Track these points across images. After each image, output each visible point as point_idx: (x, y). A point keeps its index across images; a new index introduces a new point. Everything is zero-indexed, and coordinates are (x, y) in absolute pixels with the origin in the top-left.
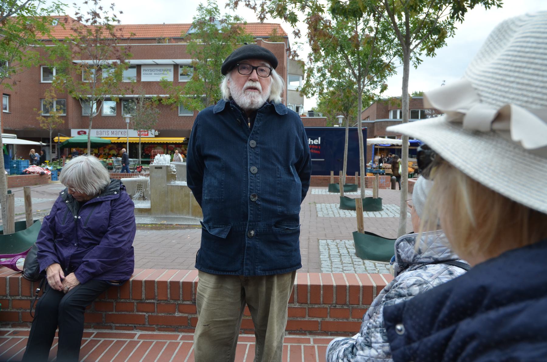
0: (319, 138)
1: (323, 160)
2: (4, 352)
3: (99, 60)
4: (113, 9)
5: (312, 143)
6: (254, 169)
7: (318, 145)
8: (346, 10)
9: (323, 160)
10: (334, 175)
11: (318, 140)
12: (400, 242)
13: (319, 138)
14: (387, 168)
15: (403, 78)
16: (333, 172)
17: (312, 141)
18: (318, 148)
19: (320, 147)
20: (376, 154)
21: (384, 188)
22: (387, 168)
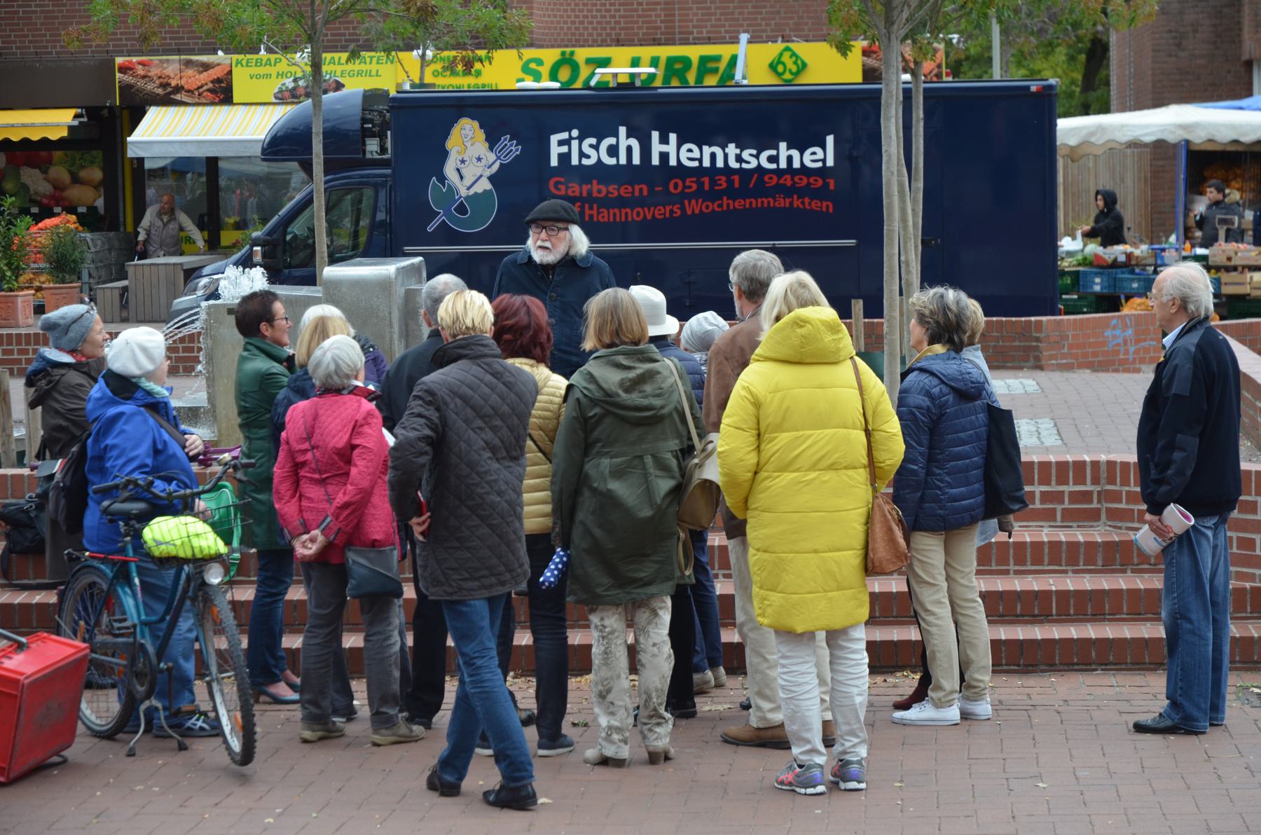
0: (830, 140)
1: (751, 186)
3: (261, 41)
4: (1140, 728)
5: (796, 165)
6: (481, 783)
7: (823, 171)
8: (213, 245)
9: (751, 186)
10: (865, 317)
11: (824, 148)
12: (1037, 616)
13: (830, 140)
14: (1235, 269)
15: (376, 89)
16: (861, 302)
17: (795, 153)
18: (826, 185)
19: (832, 183)
20: (1195, 186)
21: (1127, 371)
22: (1235, 269)
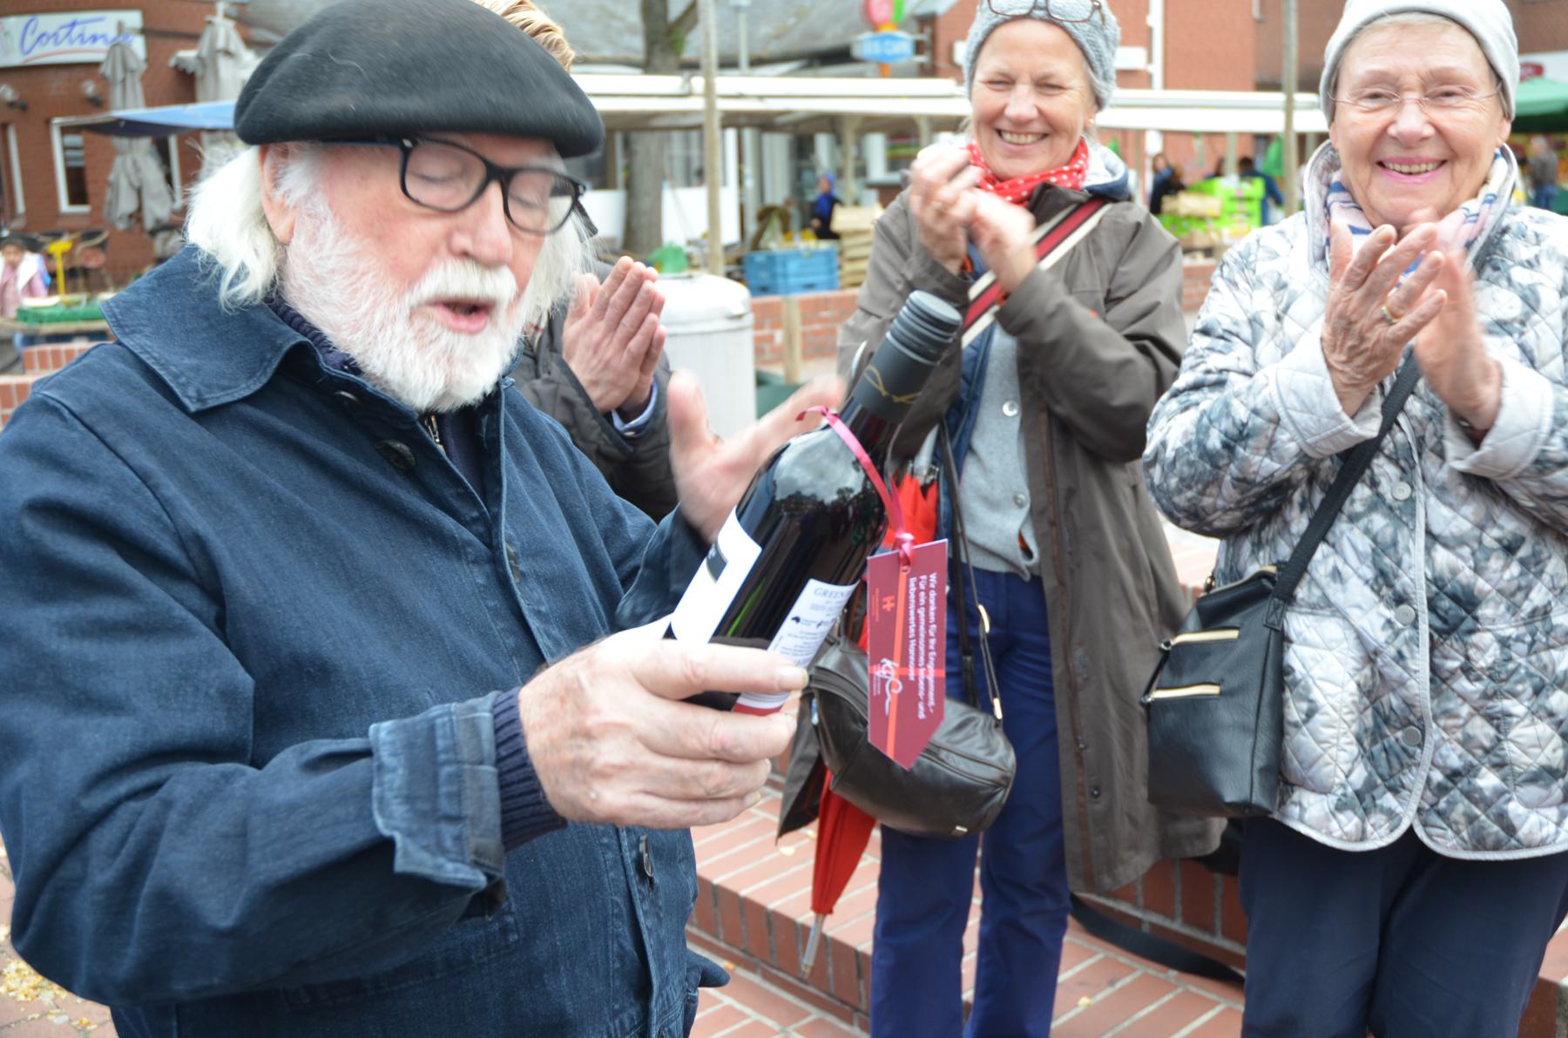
2: (1151, 1008)
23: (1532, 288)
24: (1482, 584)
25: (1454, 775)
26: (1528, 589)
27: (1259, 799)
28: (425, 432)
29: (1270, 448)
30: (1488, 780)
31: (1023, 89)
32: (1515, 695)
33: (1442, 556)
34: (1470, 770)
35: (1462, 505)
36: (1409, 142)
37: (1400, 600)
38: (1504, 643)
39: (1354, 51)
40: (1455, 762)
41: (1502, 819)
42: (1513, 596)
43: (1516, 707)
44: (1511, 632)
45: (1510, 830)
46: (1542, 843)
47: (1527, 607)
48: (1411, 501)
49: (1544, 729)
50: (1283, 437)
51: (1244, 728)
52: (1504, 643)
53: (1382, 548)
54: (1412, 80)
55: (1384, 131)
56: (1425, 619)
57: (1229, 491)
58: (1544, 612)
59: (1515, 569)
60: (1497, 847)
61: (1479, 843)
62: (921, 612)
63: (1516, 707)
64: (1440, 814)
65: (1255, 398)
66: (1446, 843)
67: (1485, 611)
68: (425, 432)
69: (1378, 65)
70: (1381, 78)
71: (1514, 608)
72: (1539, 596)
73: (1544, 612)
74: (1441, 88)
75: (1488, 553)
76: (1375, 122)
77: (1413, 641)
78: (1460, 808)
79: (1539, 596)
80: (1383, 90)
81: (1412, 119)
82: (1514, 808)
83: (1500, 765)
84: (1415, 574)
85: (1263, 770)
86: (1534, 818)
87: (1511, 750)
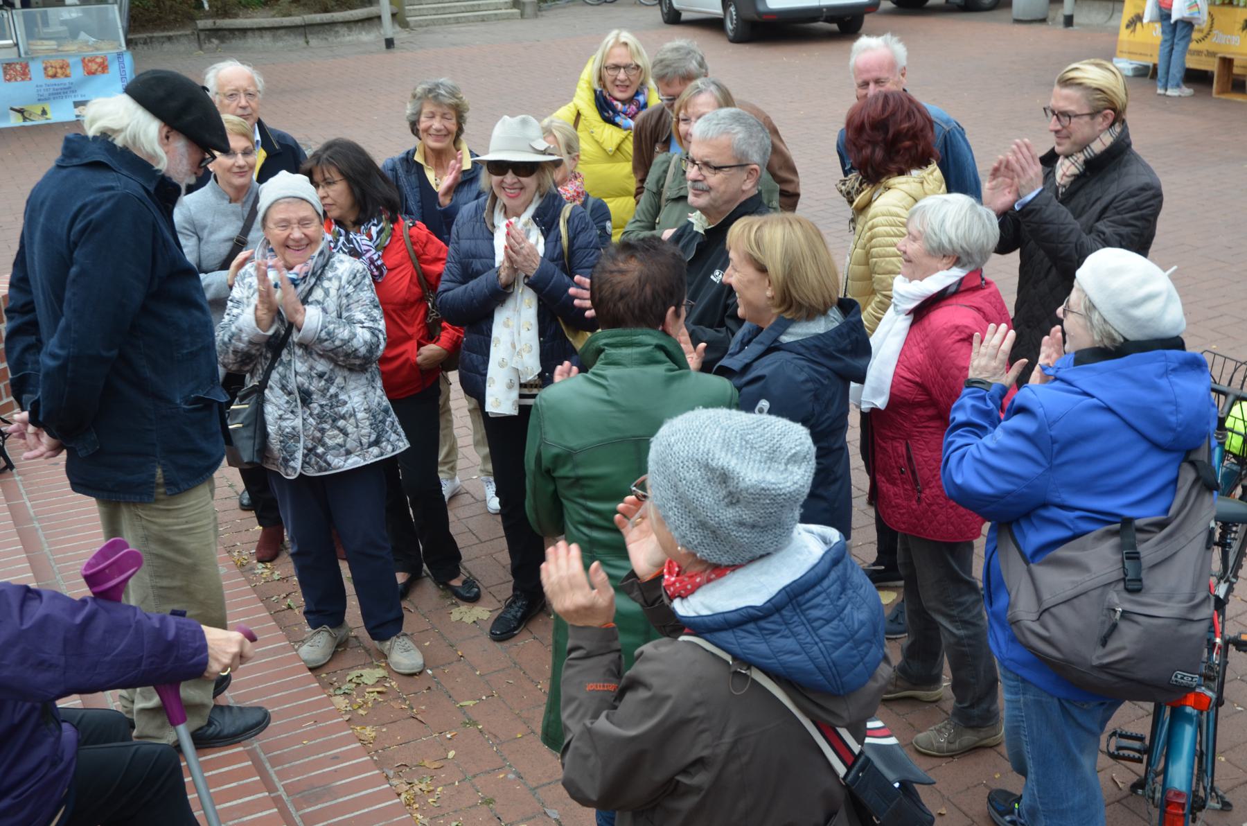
23: (328, 289)
24: (312, 388)
25: (310, 450)
26: (328, 389)
27: (256, 460)
28: (104, 208)
29: (240, 340)
30: (320, 450)
31: (872, 86)
32: (326, 422)
33: (299, 378)
34: (315, 448)
35: (659, 540)
36: (298, 241)
37: (290, 393)
38: (321, 406)
39: (272, 210)
40: (310, 446)
41: (326, 461)
42: (324, 392)
43: (327, 426)
44: (324, 403)
45: (329, 465)
46: (339, 468)
47: (329, 394)
48: (290, 361)
49: (336, 432)
50: (244, 335)
51: (249, 438)
52: (321, 406)
53: (284, 377)
54: (295, 221)
55: (288, 237)
56: (299, 401)
57: (231, 356)
58: (336, 395)
59: (323, 383)
60: (326, 470)
61: (321, 469)
62: (309, 726)
63: (327, 426)
64: (308, 463)
65: (839, 626)
66: (311, 473)
67: (315, 397)
68: (104, 208)
69: (283, 216)
70: (284, 220)
71: (324, 395)
72: (332, 390)
73: (336, 395)
74: (303, 222)
75: (312, 377)
76: (286, 233)
77: (296, 406)
78: (313, 460)
79: (332, 390)
80: (286, 224)
81: (297, 234)
82: (329, 458)
83: (324, 445)
84: (292, 386)
85: (258, 451)
86: (336, 460)
87: (327, 440)
